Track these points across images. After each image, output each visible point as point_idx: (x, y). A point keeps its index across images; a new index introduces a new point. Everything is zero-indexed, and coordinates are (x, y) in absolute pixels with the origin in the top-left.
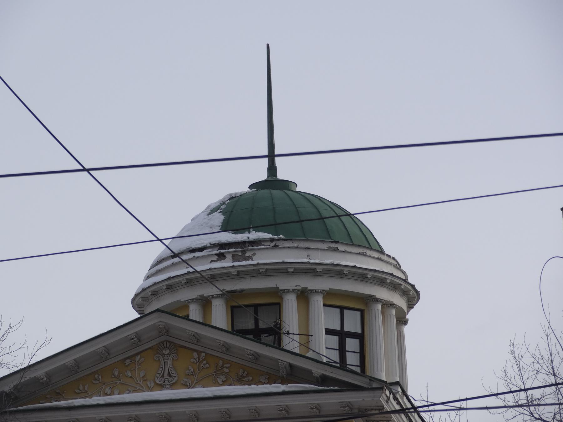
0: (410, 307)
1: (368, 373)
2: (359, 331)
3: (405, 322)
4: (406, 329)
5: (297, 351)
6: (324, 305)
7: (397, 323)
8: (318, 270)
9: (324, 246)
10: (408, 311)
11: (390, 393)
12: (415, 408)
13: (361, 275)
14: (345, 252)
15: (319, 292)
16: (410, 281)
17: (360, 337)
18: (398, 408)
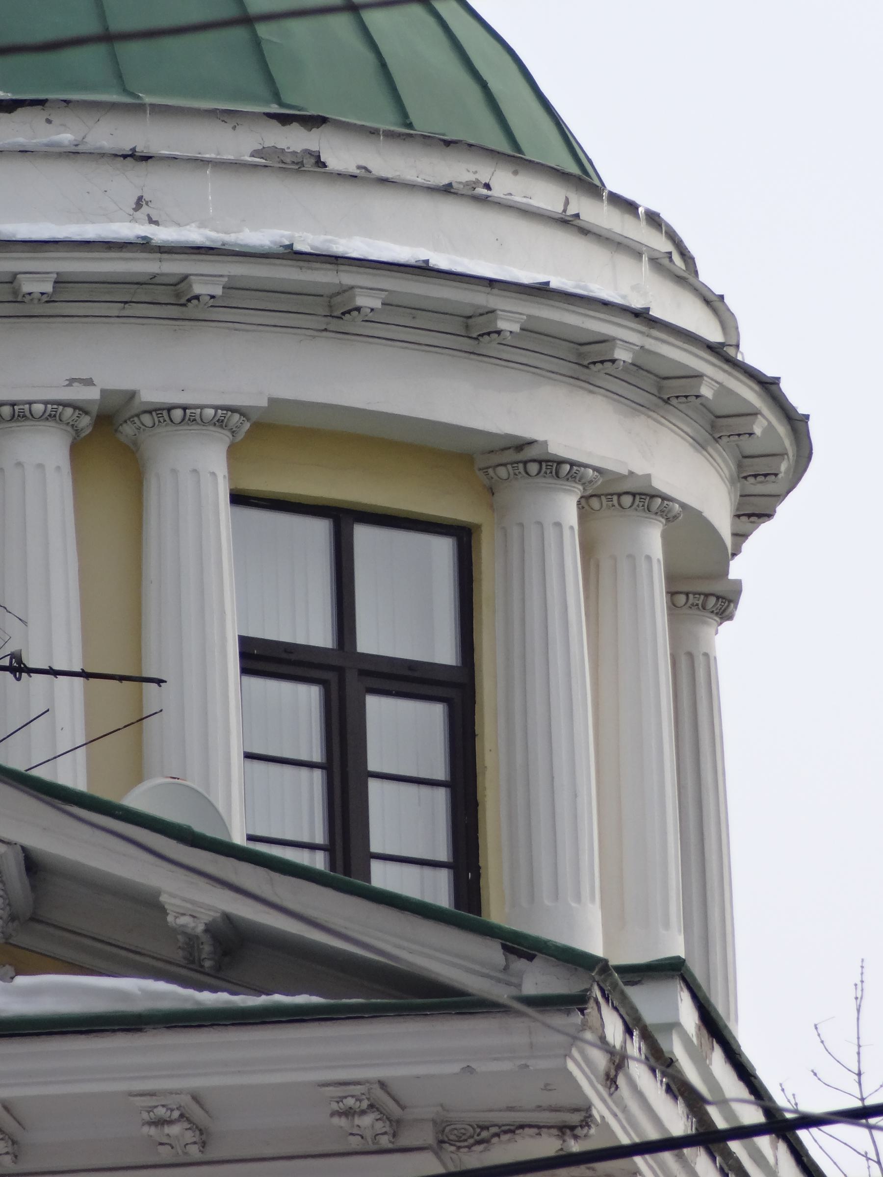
0: (753, 512)
1: (497, 910)
2: (444, 652)
3: (722, 603)
4: (728, 644)
5: (71, 775)
6: (239, 499)
7: (672, 606)
8: (198, 289)
9: (239, 143)
10: (740, 536)
11: (629, 1031)
12: (783, 1126)
13: (463, 320)
14: (360, 178)
15: (203, 422)
16: (751, 353)
17: (454, 689)
18: (677, 1121)
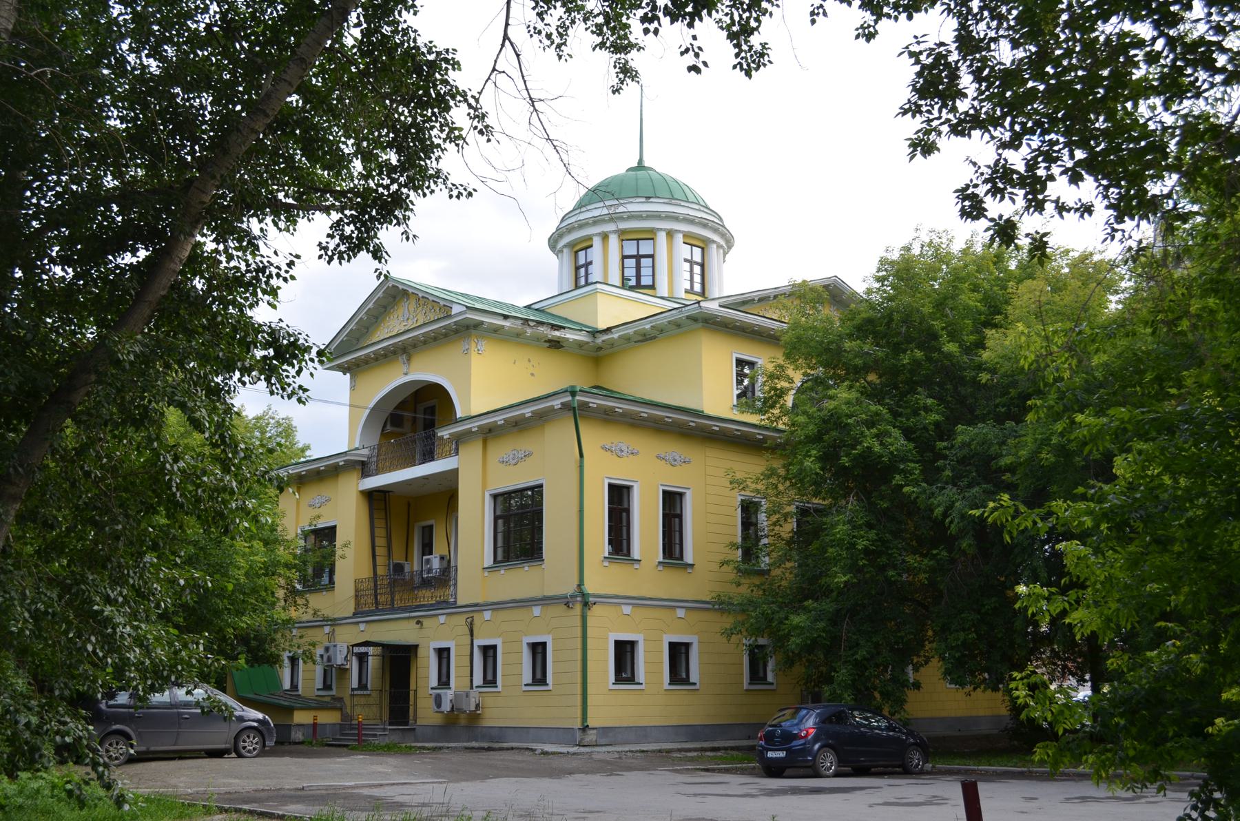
2: (651, 252)
17: (702, 265)
